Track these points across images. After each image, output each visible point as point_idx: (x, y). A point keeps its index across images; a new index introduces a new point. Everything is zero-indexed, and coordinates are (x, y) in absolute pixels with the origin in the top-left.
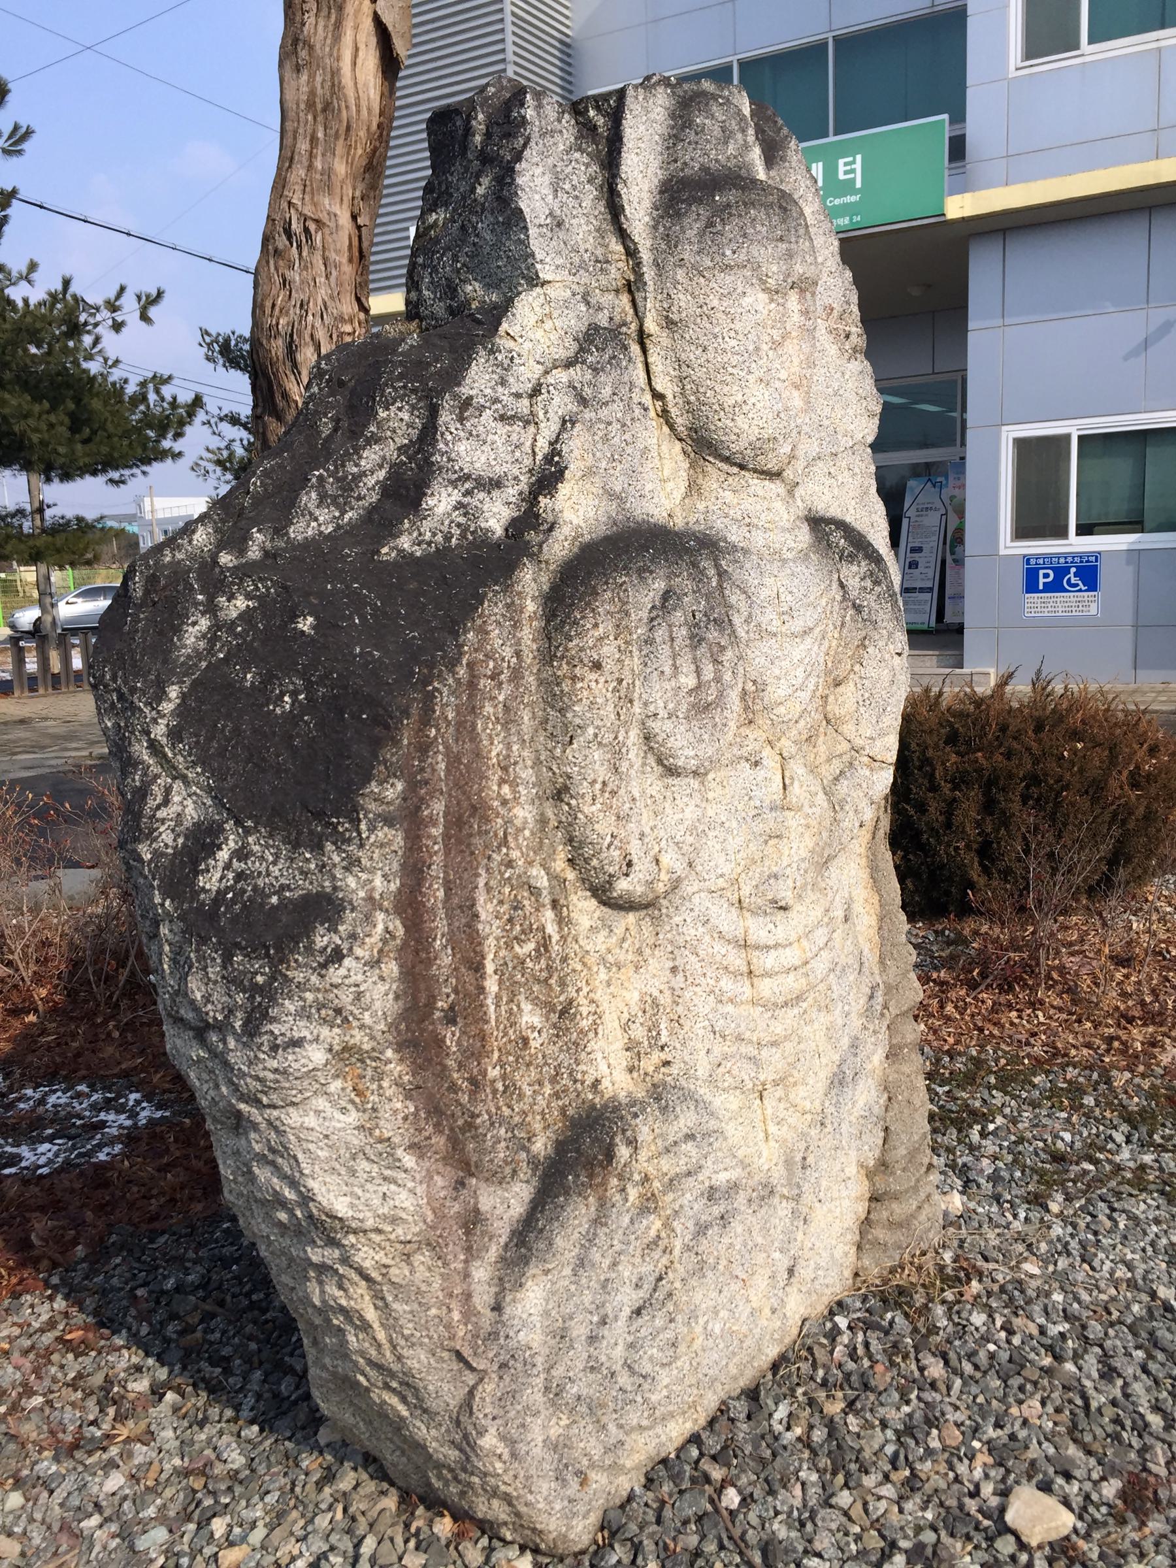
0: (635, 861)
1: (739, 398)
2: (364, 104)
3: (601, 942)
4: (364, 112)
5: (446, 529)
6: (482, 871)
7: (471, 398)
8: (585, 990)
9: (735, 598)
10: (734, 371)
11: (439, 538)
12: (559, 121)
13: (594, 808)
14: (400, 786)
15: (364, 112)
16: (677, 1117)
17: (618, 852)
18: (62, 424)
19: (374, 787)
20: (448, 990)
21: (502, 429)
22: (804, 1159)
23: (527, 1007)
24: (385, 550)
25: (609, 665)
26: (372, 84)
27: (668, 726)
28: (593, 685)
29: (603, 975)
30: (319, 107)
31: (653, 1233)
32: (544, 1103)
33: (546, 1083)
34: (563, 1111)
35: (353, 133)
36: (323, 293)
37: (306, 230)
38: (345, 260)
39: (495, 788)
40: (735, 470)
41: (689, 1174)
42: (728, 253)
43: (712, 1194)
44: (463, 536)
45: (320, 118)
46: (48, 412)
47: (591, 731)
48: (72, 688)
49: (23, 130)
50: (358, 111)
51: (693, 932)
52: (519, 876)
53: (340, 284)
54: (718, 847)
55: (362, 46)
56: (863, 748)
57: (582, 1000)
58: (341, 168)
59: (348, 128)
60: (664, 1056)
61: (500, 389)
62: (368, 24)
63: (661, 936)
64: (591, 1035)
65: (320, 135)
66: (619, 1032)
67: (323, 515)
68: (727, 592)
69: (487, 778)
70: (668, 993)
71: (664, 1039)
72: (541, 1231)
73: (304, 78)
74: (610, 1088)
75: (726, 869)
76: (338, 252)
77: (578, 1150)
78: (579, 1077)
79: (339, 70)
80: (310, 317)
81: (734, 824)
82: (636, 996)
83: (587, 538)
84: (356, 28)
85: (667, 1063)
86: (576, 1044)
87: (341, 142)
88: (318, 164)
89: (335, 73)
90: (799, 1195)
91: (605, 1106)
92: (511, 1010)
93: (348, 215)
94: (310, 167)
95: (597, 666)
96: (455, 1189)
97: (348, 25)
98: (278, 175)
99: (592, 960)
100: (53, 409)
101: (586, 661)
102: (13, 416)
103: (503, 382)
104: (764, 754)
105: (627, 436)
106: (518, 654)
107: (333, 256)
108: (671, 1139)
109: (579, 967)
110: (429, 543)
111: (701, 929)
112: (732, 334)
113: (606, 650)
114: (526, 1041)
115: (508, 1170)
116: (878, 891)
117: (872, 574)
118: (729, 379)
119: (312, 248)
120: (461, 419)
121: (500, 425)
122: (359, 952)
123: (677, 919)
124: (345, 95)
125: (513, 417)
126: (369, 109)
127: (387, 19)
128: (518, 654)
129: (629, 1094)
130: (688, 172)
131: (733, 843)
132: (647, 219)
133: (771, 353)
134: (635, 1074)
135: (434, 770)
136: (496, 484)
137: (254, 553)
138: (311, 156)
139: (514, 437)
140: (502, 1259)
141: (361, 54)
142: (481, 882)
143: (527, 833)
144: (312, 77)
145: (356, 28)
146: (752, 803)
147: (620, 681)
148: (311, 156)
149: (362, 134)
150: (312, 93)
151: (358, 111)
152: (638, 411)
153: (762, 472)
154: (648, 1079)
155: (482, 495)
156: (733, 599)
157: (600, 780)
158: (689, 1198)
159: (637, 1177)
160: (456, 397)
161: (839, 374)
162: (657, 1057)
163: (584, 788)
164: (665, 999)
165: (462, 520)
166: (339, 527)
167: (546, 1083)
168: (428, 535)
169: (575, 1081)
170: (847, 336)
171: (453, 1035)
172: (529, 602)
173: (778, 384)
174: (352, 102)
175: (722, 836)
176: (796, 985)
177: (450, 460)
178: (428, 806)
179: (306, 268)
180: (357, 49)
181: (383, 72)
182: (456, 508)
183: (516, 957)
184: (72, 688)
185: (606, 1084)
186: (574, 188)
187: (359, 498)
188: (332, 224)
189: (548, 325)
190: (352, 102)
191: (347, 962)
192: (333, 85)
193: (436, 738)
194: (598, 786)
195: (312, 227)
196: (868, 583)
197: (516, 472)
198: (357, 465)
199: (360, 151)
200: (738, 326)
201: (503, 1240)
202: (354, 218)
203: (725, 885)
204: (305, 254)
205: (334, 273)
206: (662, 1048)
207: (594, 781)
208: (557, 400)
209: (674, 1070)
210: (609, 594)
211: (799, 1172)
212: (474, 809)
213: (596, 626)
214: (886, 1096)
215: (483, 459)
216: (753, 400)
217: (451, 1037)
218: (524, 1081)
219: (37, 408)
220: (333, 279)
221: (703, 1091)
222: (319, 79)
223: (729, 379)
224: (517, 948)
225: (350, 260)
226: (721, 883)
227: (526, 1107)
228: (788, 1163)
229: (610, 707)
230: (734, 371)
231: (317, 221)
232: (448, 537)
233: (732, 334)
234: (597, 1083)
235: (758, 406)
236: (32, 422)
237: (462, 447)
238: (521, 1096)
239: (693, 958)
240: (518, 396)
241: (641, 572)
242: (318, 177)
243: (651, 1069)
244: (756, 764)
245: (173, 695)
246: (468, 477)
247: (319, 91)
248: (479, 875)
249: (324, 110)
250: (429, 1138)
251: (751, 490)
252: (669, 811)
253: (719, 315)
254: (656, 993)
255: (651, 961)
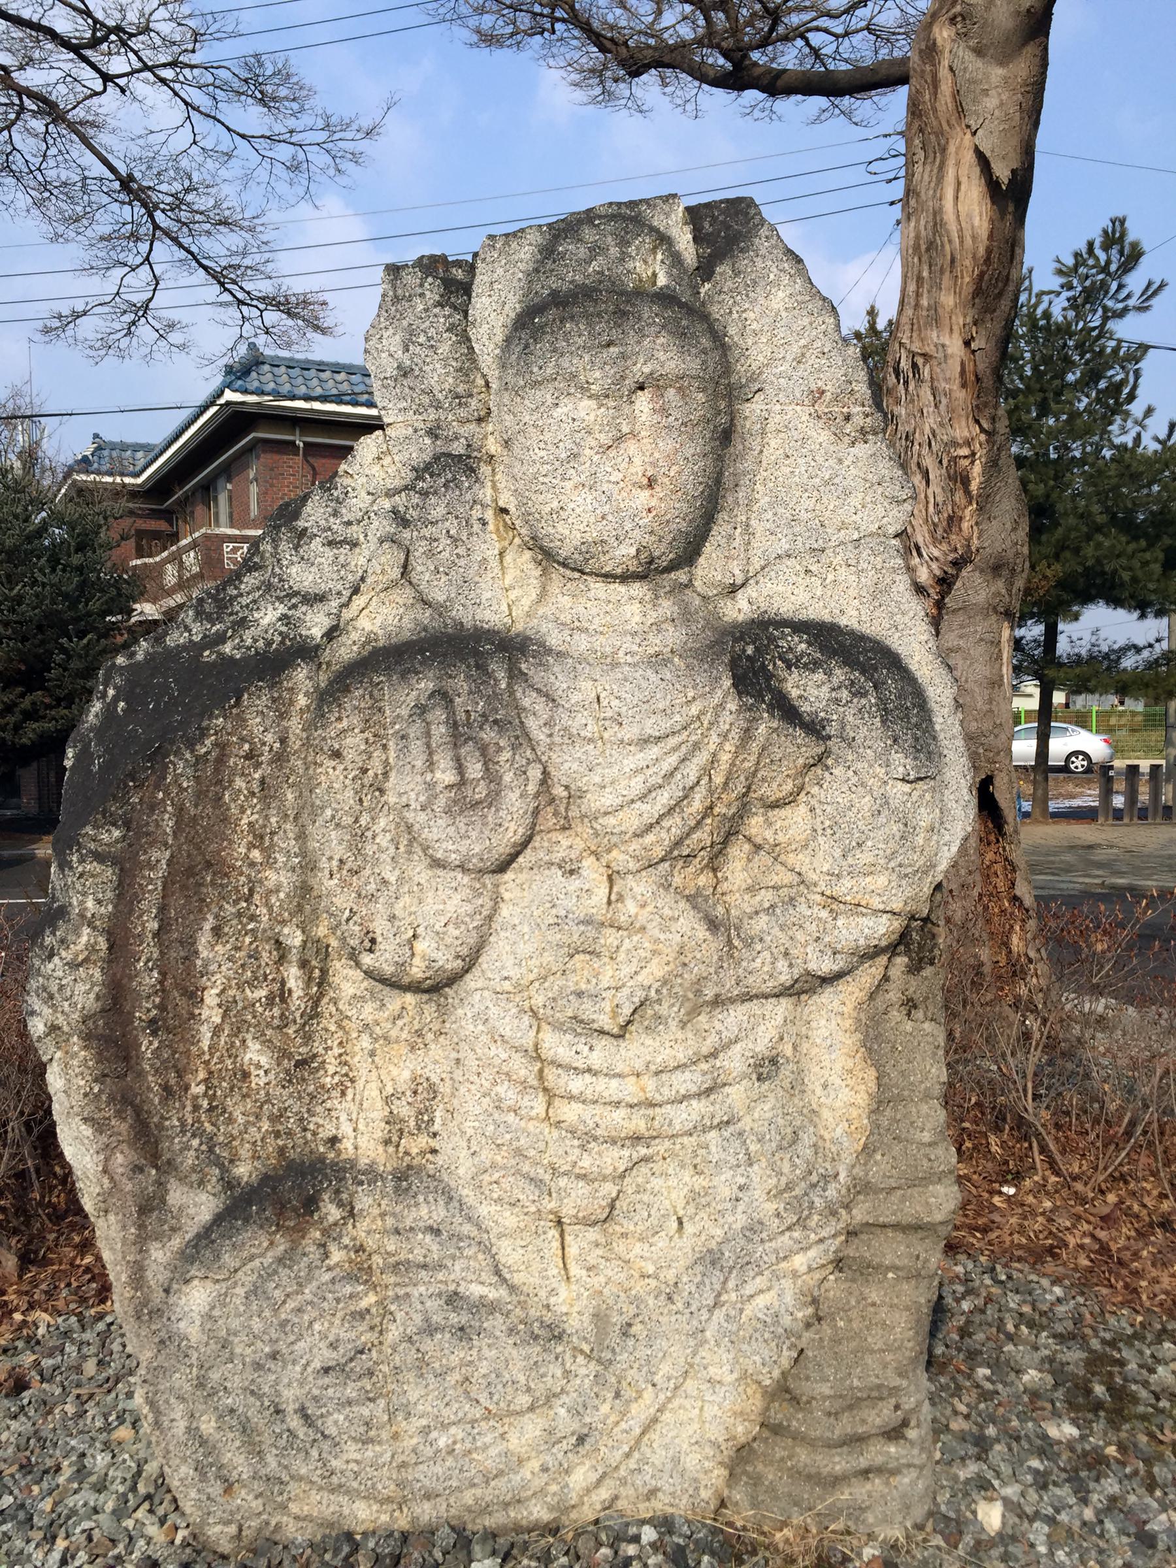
0: (379, 939)
1: (555, 504)
2: (968, 235)
3: (368, 1011)
4: (968, 241)
5: (269, 636)
6: (210, 917)
7: (306, 529)
8: (337, 1051)
9: (528, 700)
10: (546, 480)
11: (261, 644)
12: (421, 285)
13: (332, 883)
14: (117, 833)
15: (968, 241)
16: (417, 1205)
17: (357, 928)
18: (1156, 560)
19: (89, 830)
20: (149, 1006)
21: (330, 553)
22: (630, 1325)
23: (254, 1046)
24: (207, 653)
25: (349, 755)
26: (977, 212)
27: (422, 817)
28: (331, 771)
29: (366, 1042)
30: (923, 247)
31: (364, 1304)
32: (258, 1137)
33: (265, 1119)
34: (282, 1151)
35: (957, 264)
36: (931, 422)
37: (914, 366)
38: (955, 386)
39: (243, 850)
40: (577, 575)
41: (425, 1266)
42: (535, 369)
43: (453, 1299)
44: (282, 642)
45: (925, 258)
46: (1144, 551)
47: (329, 812)
48: (1158, 820)
49: (1155, 286)
50: (962, 242)
51: (471, 1027)
52: (265, 931)
53: (951, 410)
54: (508, 948)
55: (964, 180)
56: (815, 885)
57: (330, 1057)
58: (948, 300)
59: (953, 261)
60: (434, 1143)
61: (332, 520)
62: (969, 157)
63: (447, 1025)
64: (336, 1093)
65: (925, 274)
66: (379, 1104)
67: (196, 628)
68: (519, 695)
69: (231, 842)
70: (448, 1083)
71: (437, 1127)
72: (213, 1242)
73: (912, 224)
74: (351, 1150)
75: (514, 973)
76: (947, 380)
77: (274, 1189)
78: (312, 1126)
79: (941, 209)
80: (916, 447)
81: (526, 929)
82: (406, 1075)
83: (381, 644)
84: (958, 164)
85: (434, 1151)
86: (312, 1097)
87: (947, 274)
88: (924, 302)
89: (937, 213)
90: (610, 1362)
91: (334, 1164)
92: (233, 1044)
93: (960, 343)
94: (917, 306)
95: (337, 755)
96: (133, 1171)
97: (951, 162)
98: (327, 364)
99: (353, 1026)
100: (1151, 545)
101: (326, 748)
102: (1106, 557)
103: (335, 514)
104: (585, 863)
105: (461, 551)
106: (283, 741)
107: (943, 385)
108: (408, 1223)
109: (333, 1028)
110: (249, 648)
111: (480, 1027)
112: (542, 445)
113: (349, 741)
114: (246, 1075)
115: (194, 1177)
116: (877, 1066)
117: (853, 683)
118: (542, 487)
119: (920, 381)
120: (296, 547)
121: (327, 549)
122: (64, 954)
123: (460, 1012)
124: (948, 232)
125: (341, 542)
126: (974, 238)
127: (985, 149)
128: (283, 741)
129: (372, 1164)
130: (536, 300)
131: (524, 949)
132: (497, 351)
133: (596, 458)
134: (391, 1149)
135: (158, 826)
136: (321, 598)
137: (140, 657)
138: (918, 295)
139: (342, 559)
140: (182, 1252)
141: (963, 187)
142: (207, 926)
143: (282, 895)
144: (918, 221)
145: (958, 164)
146: (554, 911)
147: (365, 771)
148: (918, 295)
149: (967, 263)
150: (918, 237)
151: (962, 242)
152: (477, 527)
153: (606, 576)
154: (407, 1158)
155: (304, 608)
156: (526, 702)
157: (337, 857)
158: (423, 1289)
159: (346, 1241)
160: (293, 529)
161: (832, 462)
162: (423, 1141)
163: (324, 863)
164: (445, 1089)
165: (284, 629)
166: (205, 636)
167: (265, 1119)
168: (249, 642)
169: (305, 1130)
170: (848, 418)
171: (151, 1043)
172: (301, 696)
173: (605, 487)
174: (955, 235)
175: (513, 938)
176: (626, 1124)
177: (281, 580)
178: (145, 853)
179: (912, 401)
180: (959, 184)
181: (992, 198)
182: (280, 619)
183: (245, 999)
184: (1158, 820)
185: (347, 1145)
186: (429, 339)
187: (231, 614)
188: (940, 355)
189: (387, 460)
190: (955, 235)
191: (56, 959)
192: (935, 224)
193: (163, 800)
194: (335, 863)
195: (920, 361)
196: (844, 694)
197: (339, 587)
198: (236, 588)
199: (967, 279)
200: (547, 436)
201: (188, 1237)
202: (967, 344)
203: (510, 989)
204: (911, 387)
205: (944, 401)
206: (435, 1135)
207: (330, 859)
208: (376, 523)
209: (440, 1160)
210: (361, 691)
211: (614, 1338)
212: (209, 864)
213: (339, 719)
214: (810, 1310)
215: (311, 578)
216: (572, 505)
217: (147, 1045)
218: (239, 1111)
219: (1132, 547)
220: (942, 407)
221: (468, 1194)
222: (922, 222)
223: (542, 487)
224: (248, 991)
225: (964, 385)
226: (507, 986)
227: (235, 1132)
228: (600, 1318)
229: (349, 793)
230: (546, 480)
231: (924, 355)
232: (269, 643)
233: (542, 445)
234: (333, 1141)
235: (578, 510)
236: (1123, 561)
237: (294, 570)
238: (230, 1120)
239: (471, 1055)
240: (349, 523)
241: (403, 676)
242: (925, 313)
243: (414, 1151)
244: (572, 872)
245: (70, 755)
246: (297, 593)
247: (923, 233)
248: (205, 919)
249: (928, 250)
250: (109, 1119)
251: (591, 594)
252: (430, 900)
253: (531, 429)
254: (435, 1079)
255: (433, 1046)
